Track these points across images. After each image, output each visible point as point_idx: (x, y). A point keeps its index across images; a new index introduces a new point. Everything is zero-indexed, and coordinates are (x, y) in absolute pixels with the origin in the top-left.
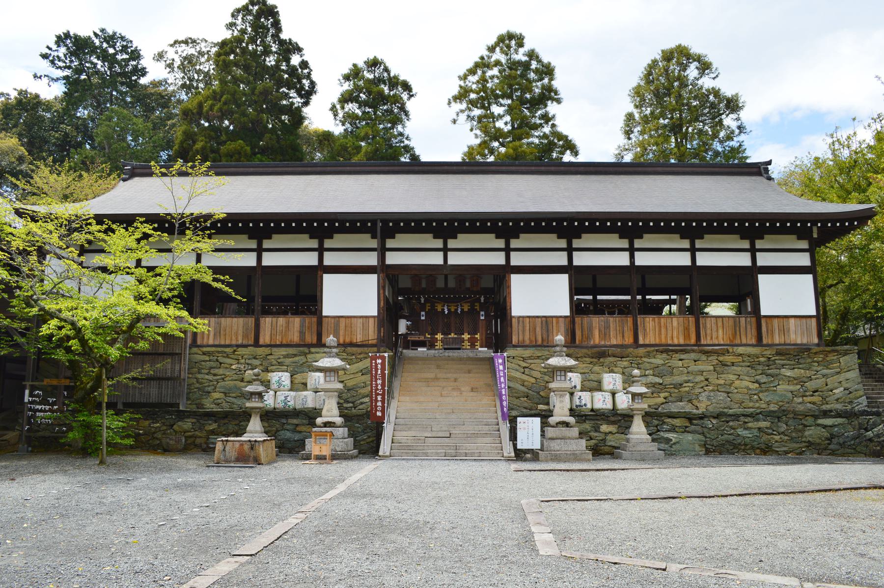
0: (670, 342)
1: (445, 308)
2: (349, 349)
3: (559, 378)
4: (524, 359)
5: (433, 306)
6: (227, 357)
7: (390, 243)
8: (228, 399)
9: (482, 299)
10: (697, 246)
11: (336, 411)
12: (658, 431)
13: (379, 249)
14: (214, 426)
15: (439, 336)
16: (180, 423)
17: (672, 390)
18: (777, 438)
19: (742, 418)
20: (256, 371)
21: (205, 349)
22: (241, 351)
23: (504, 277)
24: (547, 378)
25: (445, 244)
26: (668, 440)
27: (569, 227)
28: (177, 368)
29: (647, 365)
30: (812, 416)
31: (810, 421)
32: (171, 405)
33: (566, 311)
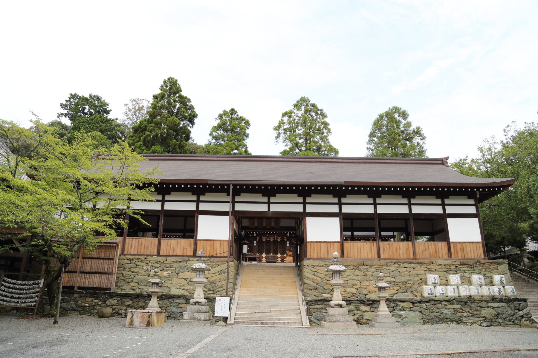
0: (399, 257)
1: (268, 237)
2: (212, 259)
3: (336, 277)
4: (314, 267)
5: (261, 238)
6: (141, 261)
7: (237, 199)
8: (140, 287)
9: (288, 235)
10: (412, 202)
11: (202, 296)
12: (394, 310)
13: (231, 202)
14: (130, 302)
15: (264, 255)
16: (110, 300)
17: (401, 285)
18: (465, 314)
19: (444, 303)
20: (156, 270)
21: (128, 257)
22: (149, 258)
23: (302, 219)
24: (327, 278)
25: (269, 199)
26: (400, 316)
27: (339, 191)
28: (111, 266)
29: (386, 271)
30: (485, 301)
31: (484, 304)
32: (106, 289)
33: (338, 239)
